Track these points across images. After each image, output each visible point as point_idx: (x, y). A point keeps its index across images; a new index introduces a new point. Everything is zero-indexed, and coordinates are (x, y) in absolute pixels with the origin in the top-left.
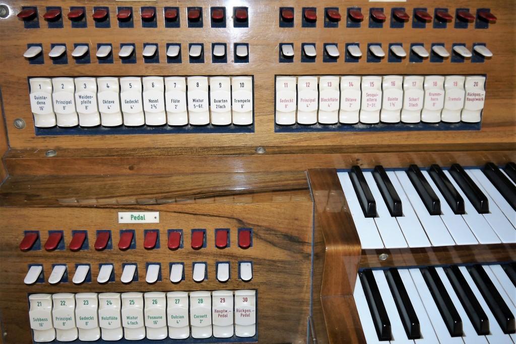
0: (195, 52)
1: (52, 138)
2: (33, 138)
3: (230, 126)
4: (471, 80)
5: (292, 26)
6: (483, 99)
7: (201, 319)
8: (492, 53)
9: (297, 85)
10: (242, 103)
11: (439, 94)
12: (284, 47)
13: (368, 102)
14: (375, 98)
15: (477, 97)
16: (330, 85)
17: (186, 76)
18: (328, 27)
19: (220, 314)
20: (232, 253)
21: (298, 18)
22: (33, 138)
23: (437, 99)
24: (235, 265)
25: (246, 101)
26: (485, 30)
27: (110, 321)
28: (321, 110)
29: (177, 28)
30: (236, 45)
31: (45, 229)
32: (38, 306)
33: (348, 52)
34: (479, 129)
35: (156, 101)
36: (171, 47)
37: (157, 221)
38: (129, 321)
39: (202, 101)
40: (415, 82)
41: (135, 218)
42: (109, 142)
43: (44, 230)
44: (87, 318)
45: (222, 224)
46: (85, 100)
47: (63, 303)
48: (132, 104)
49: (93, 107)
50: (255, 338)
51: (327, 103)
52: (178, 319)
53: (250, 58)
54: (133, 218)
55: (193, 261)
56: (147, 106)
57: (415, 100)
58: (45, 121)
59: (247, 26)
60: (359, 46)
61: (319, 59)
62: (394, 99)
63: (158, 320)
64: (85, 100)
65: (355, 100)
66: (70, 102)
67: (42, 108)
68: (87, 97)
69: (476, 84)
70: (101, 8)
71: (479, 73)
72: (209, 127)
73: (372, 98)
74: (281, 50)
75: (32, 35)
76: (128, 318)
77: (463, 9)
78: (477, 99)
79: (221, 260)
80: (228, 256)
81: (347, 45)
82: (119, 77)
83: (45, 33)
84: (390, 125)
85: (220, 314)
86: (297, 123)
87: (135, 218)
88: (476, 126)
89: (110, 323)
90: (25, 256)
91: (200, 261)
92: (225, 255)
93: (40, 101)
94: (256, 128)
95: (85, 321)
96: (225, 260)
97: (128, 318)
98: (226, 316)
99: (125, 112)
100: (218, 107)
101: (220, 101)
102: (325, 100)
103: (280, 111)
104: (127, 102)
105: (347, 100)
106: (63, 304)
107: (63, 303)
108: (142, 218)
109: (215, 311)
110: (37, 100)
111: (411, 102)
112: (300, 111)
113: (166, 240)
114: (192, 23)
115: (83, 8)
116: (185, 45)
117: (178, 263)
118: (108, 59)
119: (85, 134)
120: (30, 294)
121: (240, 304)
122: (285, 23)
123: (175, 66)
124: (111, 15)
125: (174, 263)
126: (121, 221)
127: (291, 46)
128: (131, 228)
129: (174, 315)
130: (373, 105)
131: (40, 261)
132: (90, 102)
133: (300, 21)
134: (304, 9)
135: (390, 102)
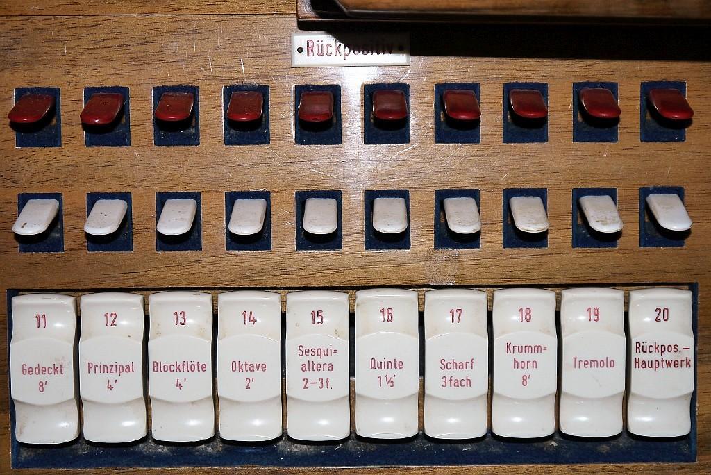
0: (247, 222)
4: (645, 301)
6: (688, 363)
8: (691, 218)
9: (421, 316)
11: (539, 348)
12: (516, 202)
13: (307, 374)
14: (326, 360)
15: (668, 356)
16: (180, 320)
18: (169, 145)
23: (535, 363)
26: (674, 145)
27: (181, 375)
28: (498, 395)
30: (370, 197)
34: (690, 459)
40: (460, 311)
44: (44, 370)
51: (172, 377)
53: (413, 236)
57: (462, 366)
59: (404, 139)
60: (681, 196)
61: (493, 239)
62: (389, 364)
65: (264, 367)
68: (321, 352)
69: (664, 317)
72: (417, 444)
73: (316, 359)
74: (440, 208)
77: (595, 84)
78: (669, 364)
81: (645, 192)
88: (684, 448)
95: (36, 379)
99: (567, 392)
100: (109, 368)
102: (167, 368)
103: (504, 394)
105: (237, 366)
111: (447, 373)
116: (144, 203)
118: (119, 240)
120: (15, 292)
123: (253, 257)
124: (65, 110)
127: (538, 200)
130: (324, 383)
132: (331, 367)
135: (377, 372)
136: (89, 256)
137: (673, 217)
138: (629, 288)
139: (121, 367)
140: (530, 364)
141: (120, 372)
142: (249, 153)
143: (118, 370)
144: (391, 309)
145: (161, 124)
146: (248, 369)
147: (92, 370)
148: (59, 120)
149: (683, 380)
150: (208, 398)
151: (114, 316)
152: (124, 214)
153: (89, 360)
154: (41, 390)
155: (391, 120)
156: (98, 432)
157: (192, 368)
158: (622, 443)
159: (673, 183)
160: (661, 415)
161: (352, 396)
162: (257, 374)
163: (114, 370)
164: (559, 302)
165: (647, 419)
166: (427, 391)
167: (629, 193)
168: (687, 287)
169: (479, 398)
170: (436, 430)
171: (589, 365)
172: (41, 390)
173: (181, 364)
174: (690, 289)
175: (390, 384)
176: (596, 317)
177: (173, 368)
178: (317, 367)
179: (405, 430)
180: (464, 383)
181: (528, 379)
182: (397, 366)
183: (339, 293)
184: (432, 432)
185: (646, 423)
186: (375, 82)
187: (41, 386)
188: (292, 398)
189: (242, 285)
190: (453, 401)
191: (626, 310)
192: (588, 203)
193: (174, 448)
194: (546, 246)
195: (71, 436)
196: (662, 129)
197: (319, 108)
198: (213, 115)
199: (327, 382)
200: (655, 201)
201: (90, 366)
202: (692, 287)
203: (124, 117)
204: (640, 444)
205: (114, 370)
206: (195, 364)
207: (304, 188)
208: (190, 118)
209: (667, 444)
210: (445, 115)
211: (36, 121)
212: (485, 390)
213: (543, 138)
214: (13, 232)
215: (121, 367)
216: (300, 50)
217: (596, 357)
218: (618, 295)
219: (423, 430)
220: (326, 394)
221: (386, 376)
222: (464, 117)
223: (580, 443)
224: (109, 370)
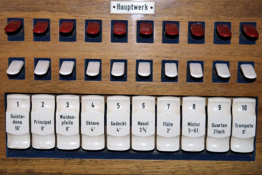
0: (118, 70)
1: (24, 160)
2: (3, 160)
3: (79, 151)
5: (177, 42)
9: (181, 107)
10: (243, 129)
17: (106, 96)
21: (209, 33)
22: (3, 160)
25: (248, 126)
28: (233, 137)
29: (175, 44)
33: (240, 72)
35: (146, 124)
36: (115, 64)
39: (198, 125)
42: (88, 167)
44: (119, 124)
46: (67, 120)
48: (118, 127)
49: (74, 129)
56: (136, 129)
58: (19, 142)
61: (183, 79)
64: (67, 120)
65: (98, 124)
66: (49, 123)
67: (17, 128)
68: (69, 117)
70: (94, 21)
71: (219, 95)
74: (163, 67)
75: (16, 49)
76: (189, 124)
81: (215, 62)
82: (207, 97)
83: (29, 47)
84: (65, 152)
93: (17, 120)
94: (257, 156)
95: (116, 127)
97: (189, 124)
100: (216, 132)
101: (218, 126)
103: (14, 134)
104: (113, 124)
105: (113, 124)
110: (13, 119)
112: (209, 137)
114: (88, 38)
115: (74, 21)
116: (55, 62)
118: (46, 77)
119: (61, 158)
122: (116, 39)
132: (72, 123)
133: (161, 37)
134: (190, 24)
135: (214, 128)
136: (35, 82)
137: (249, 72)
138: (107, 96)
139: (117, 125)
141: (46, 124)
142: (119, 45)
143: (45, 123)
144: (144, 103)
145: (62, 34)
146: (92, 124)
147: (36, 123)
148: (50, 33)
149: (251, 132)
150: (78, 134)
151: (43, 103)
152: (22, 67)
153: (37, 120)
154: (42, 129)
155: (252, 37)
156: (38, 145)
157: (46, 123)
158: (229, 154)
162: (96, 126)
163: (44, 123)
164: (131, 101)
165: (238, 146)
166: (157, 134)
167: (183, 63)
172: (42, 129)
173: (91, 122)
174: (255, 99)
175: (145, 131)
177: (122, 124)
178: (171, 125)
179: (150, 147)
180: (222, 132)
182: (171, 125)
184: (109, 148)
185: (237, 147)
186: (140, 20)
188: (158, 136)
189: (190, 95)
190: (192, 138)
191: (206, 105)
192: (243, 67)
193: (138, 153)
194: (203, 82)
195: (77, 146)
196: (219, 39)
197: (119, 30)
198: (81, 31)
199: (197, 130)
200: (243, 67)
201: (35, 121)
202: (256, 98)
203: (22, 29)
204: (110, 153)
205: (44, 123)
206: (169, 123)
208: (72, 32)
209: (144, 153)
210: (166, 33)
211: (15, 31)
212: (204, 133)
213: (177, 42)
214: (7, 73)
215: (117, 125)
216: (114, 7)
217: (225, 123)
218: (229, 100)
219: (206, 149)
220: (196, 135)
221: (144, 128)
222: (146, 33)
223: (24, 151)
224: (44, 122)
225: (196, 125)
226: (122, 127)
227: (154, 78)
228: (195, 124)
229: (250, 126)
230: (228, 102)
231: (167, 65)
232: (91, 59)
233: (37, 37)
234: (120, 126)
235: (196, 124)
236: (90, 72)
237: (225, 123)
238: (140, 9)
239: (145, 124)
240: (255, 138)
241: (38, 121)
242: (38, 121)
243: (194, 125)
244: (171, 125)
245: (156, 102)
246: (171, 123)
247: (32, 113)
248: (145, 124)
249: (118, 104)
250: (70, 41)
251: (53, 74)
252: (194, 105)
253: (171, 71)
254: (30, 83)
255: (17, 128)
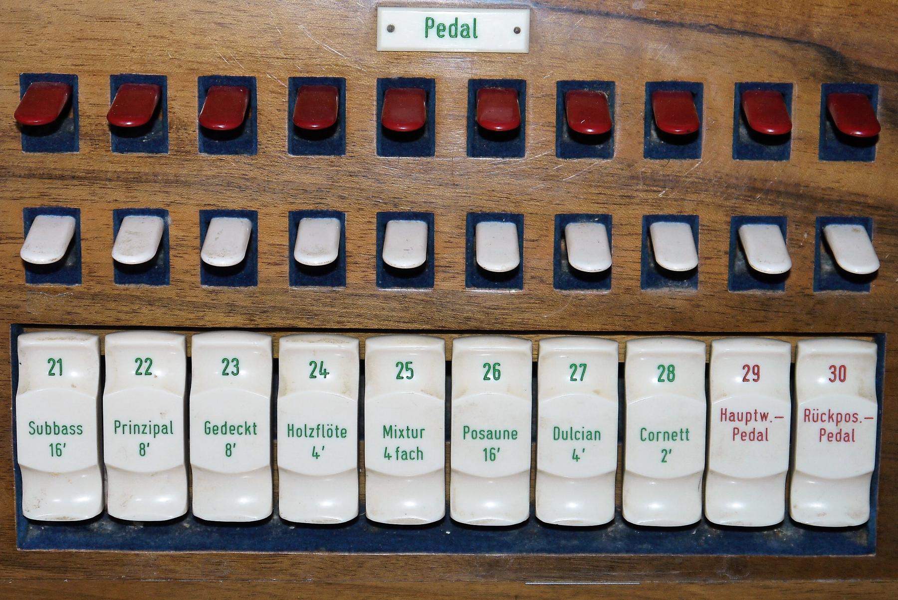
7: (668, 445)
10: (662, 444)
11: (853, 417)
19: (742, 426)
20: (797, 185)
24: (809, 218)
27: (318, 442)
28: (713, 472)
31: (98, 66)
32: (51, 374)
37: (519, 44)
38: (392, 443)
40: (585, 366)
41: (440, 30)
43: (94, 74)
44: (233, 429)
45: (764, 65)
47: (145, 365)
50: (862, 540)
52: (578, 445)
54: (433, 32)
55: (648, 211)
58: (57, 493)
63: (502, 443)
66: (166, 429)
74: (561, 235)
76: (388, 431)
79: (751, 210)
80: (779, 193)
81: (649, 220)
82: (275, 331)
84: (465, 531)
85: (742, 426)
86: (447, 519)
87: (440, 30)
89: (318, 450)
90: (14, 175)
91: (673, 211)
92: (773, 192)
95: (222, 440)
96: (767, 210)
97: (388, 431)
98: (761, 437)
100: (142, 428)
105: (210, 429)
106: (143, 370)
107: (145, 365)
108: (468, 32)
109: (723, 413)
113: (549, 124)
117: (589, 218)
118: (153, 271)
120: (20, 328)
121: (815, 383)
122: (485, 143)
125: (575, 218)
126: (386, 42)
128: (418, 71)
129: (565, 428)
131: (71, 195)
136: (204, 292)
137: (854, 251)
138: (277, 334)
140: (661, 436)
141: (155, 433)
142: (232, 164)
144: (499, 365)
147: (120, 430)
149: (861, 456)
151: (400, 366)
153: (126, 424)
159: (511, 209)
160: (835, 499)
161: (448, 470)
167: (628, 216)
168: (871, 338)
169: (693, 475)
170: (382, 511)
171: (747, 438)
176: (756, 377)
177: (242, 430)
180: (414, 455)
181: (146, 448)
182: (339, 434)
183: (517, 340)
187: (229, 449)
188: (457, 472)
202: (878, 338)
206: (334, 428)
207: (477, 210)
217: (744, 430)
224: (141, 431)
225: (410, 435)
226: (332, 443)
227: (264, 270)
228: (408, 429)
229: (679, 435)
230: (781, 355)
231: (484, 230)
232: (134, 209)
233: (34, 140)
234: (326, 441)
235: (410, 432)
236: (219, 256)
237: (744, 430)
238: (441, 33)
239: (486, 434)
240: (874, 476)
241: (128, 424)
242: (128, 424)
243: (405, 433)
244: (339, 432)
245: (276, 356)
246: (340, 428)
247: (280, 400)
248: (479, 435)
249: (410, 366)
250: (845, 160)
251: (178, 263)
252: (671, 369)
253: (497, 250)
254: (93, 297)
255: (57, 449)
